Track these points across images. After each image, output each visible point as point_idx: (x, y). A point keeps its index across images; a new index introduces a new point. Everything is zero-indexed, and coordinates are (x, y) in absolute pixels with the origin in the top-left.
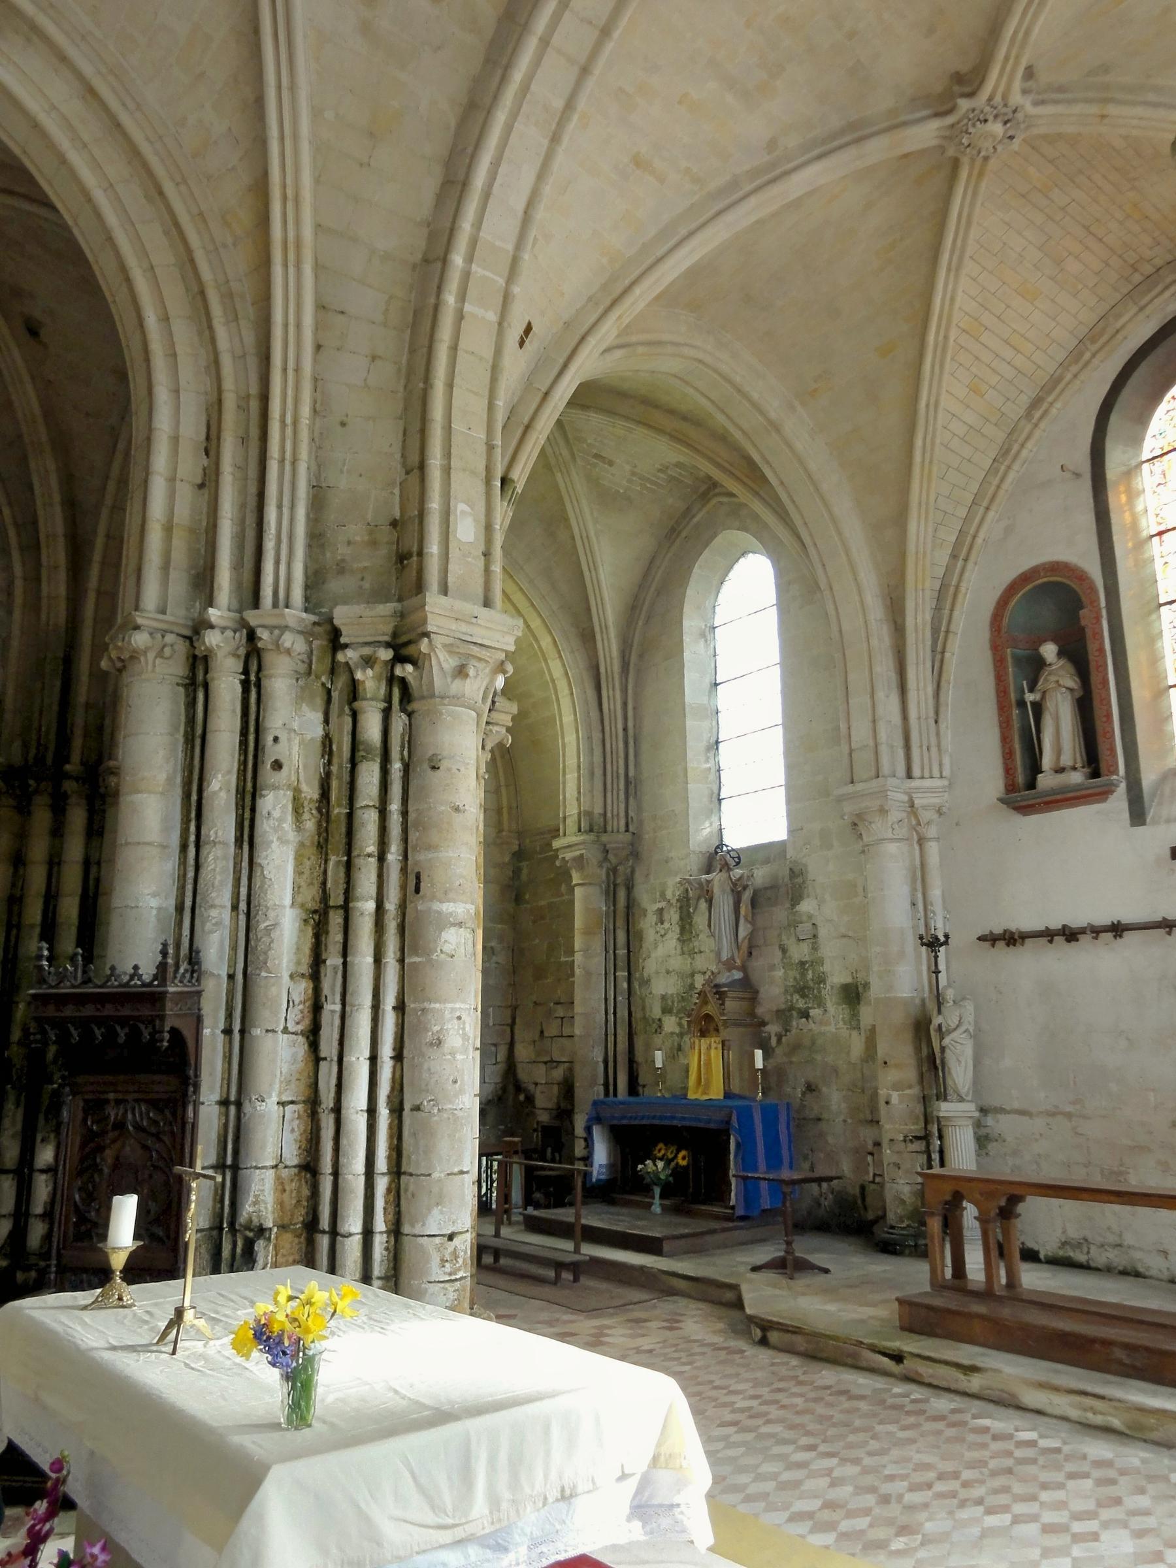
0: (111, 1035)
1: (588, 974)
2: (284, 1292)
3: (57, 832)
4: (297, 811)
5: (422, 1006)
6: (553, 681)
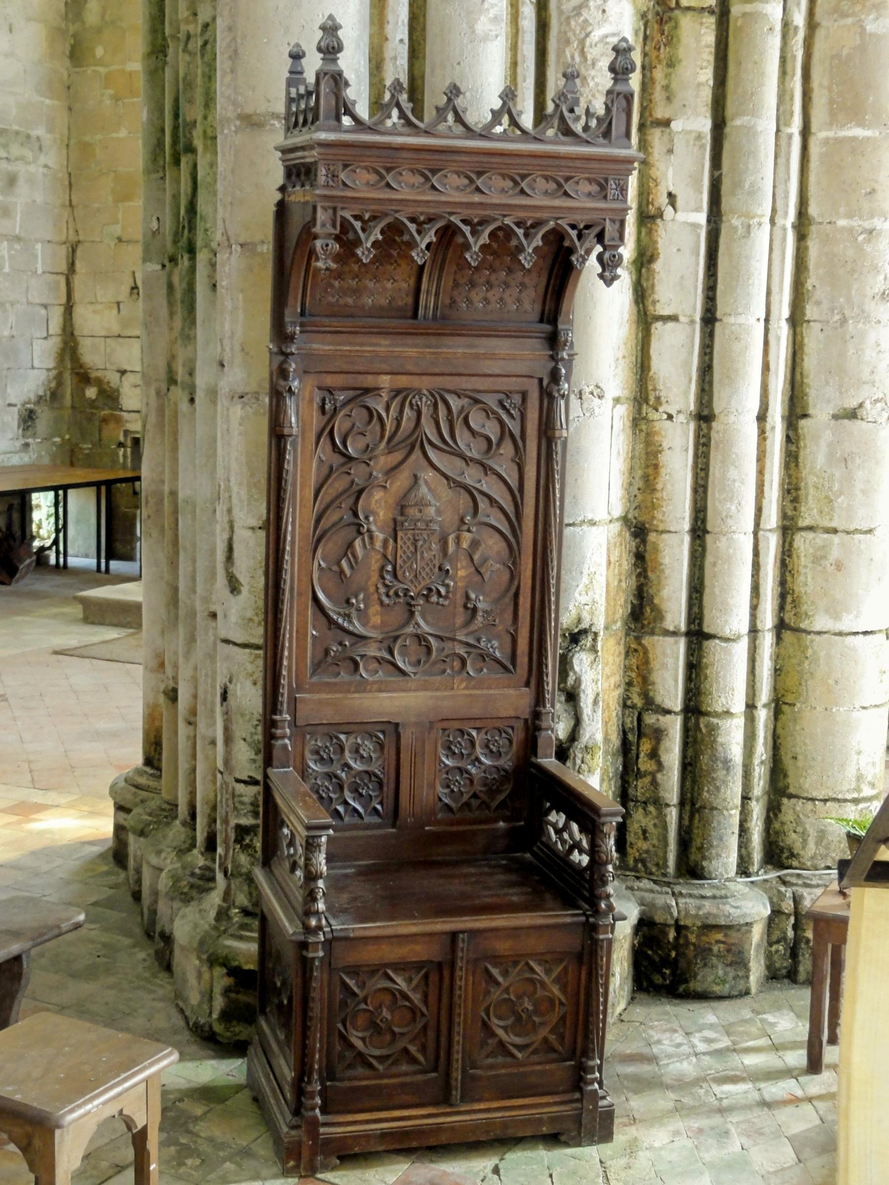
5: (867, 225)
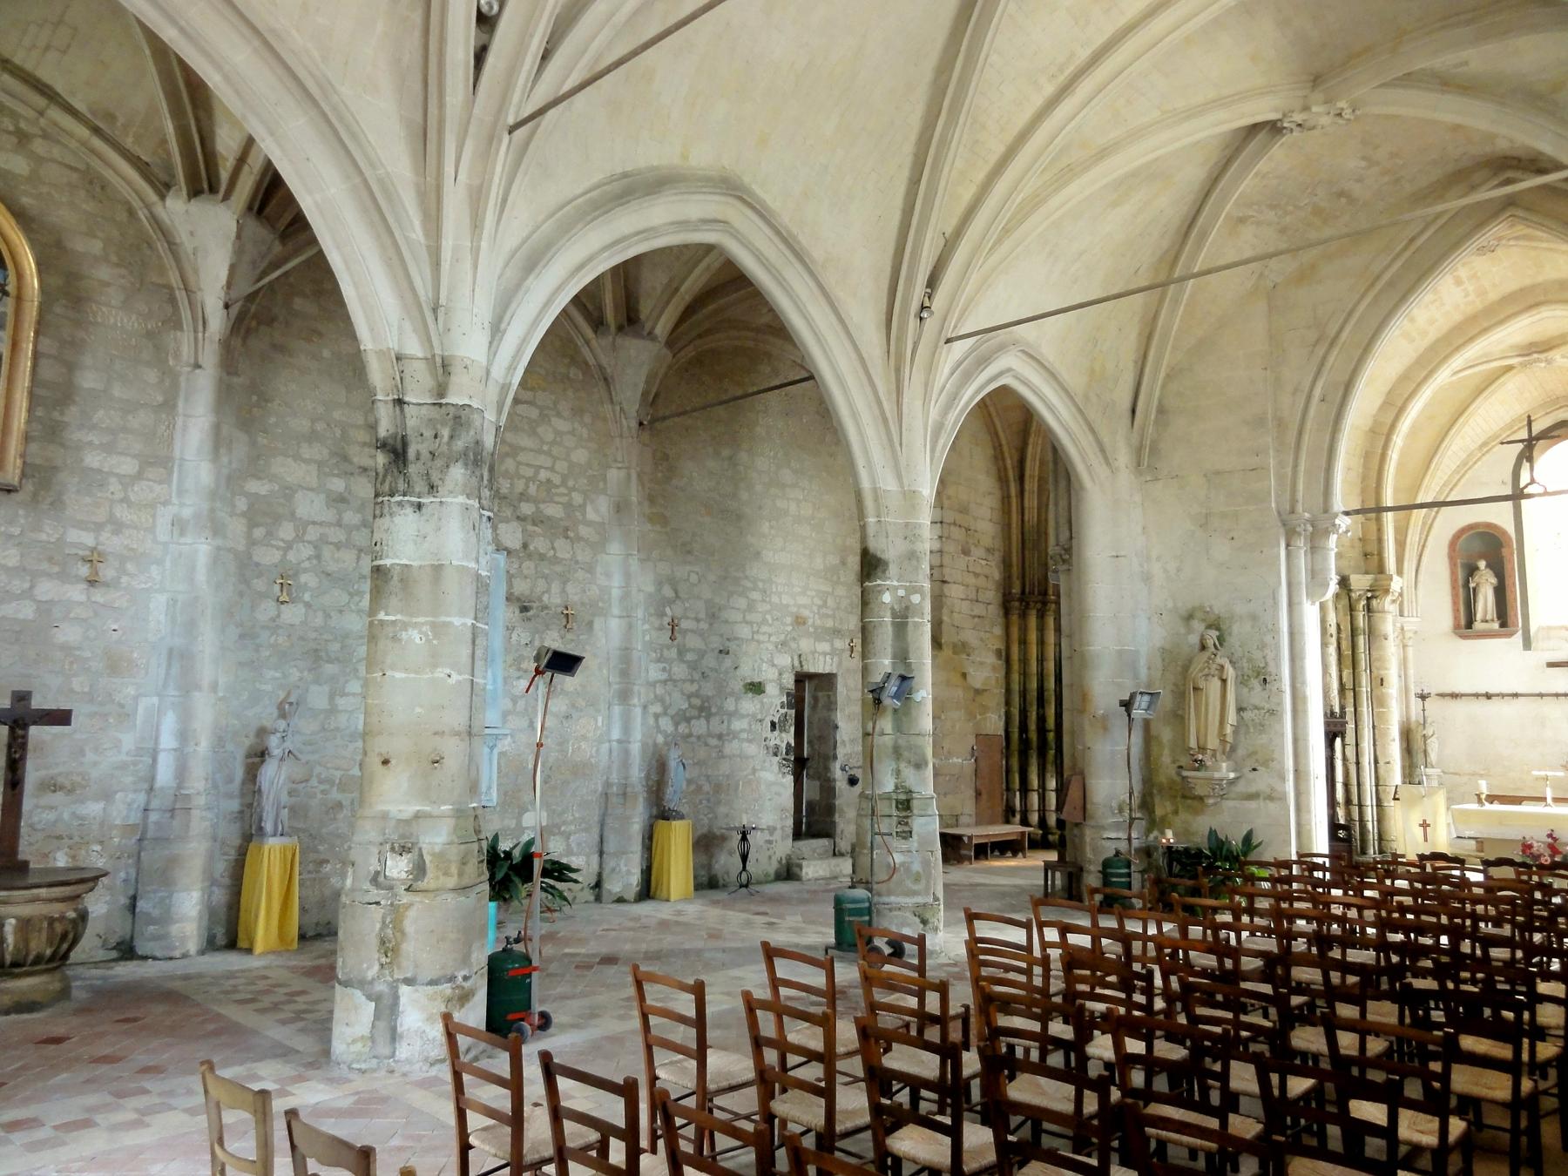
3: (1041, 629)
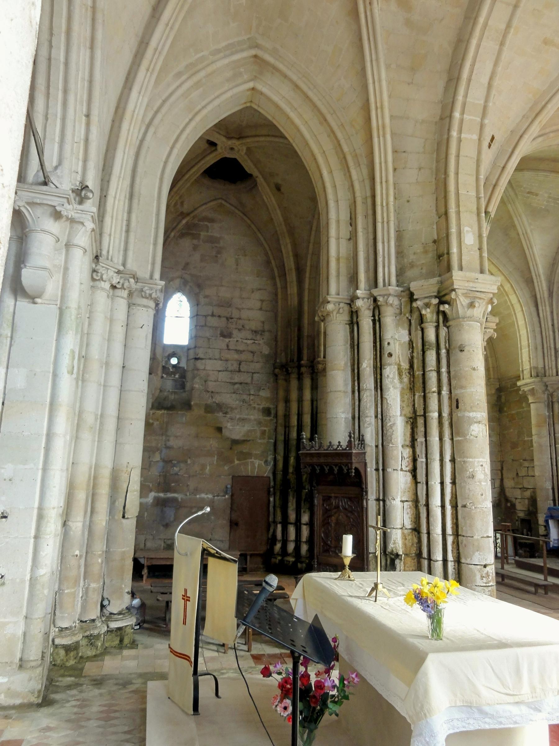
0: (331, 470)
1: (540, 446)
2: (425, 582)
3: (301, 389)
4: (400, 374)
5: (463, 460)
6: (512, 305)
